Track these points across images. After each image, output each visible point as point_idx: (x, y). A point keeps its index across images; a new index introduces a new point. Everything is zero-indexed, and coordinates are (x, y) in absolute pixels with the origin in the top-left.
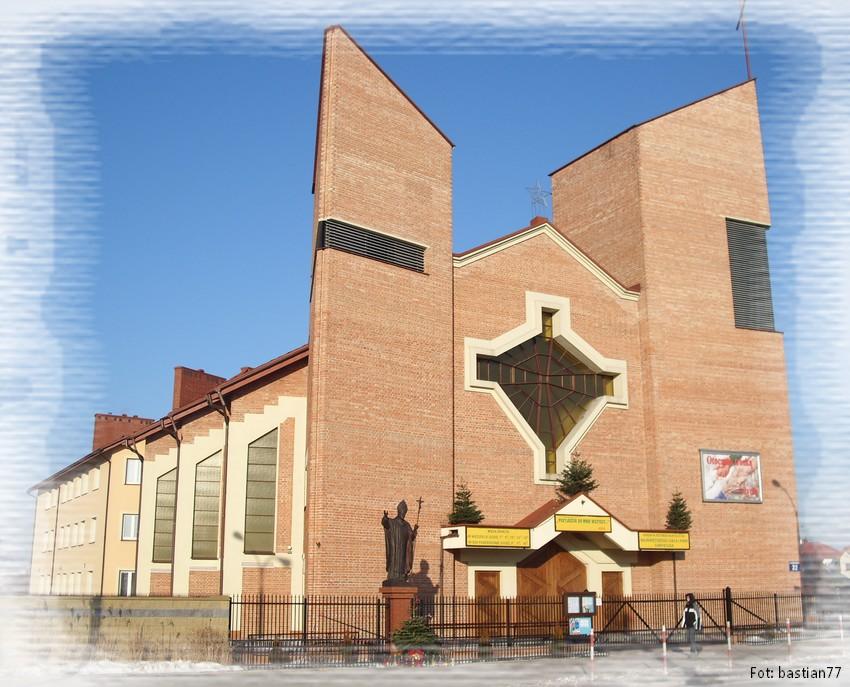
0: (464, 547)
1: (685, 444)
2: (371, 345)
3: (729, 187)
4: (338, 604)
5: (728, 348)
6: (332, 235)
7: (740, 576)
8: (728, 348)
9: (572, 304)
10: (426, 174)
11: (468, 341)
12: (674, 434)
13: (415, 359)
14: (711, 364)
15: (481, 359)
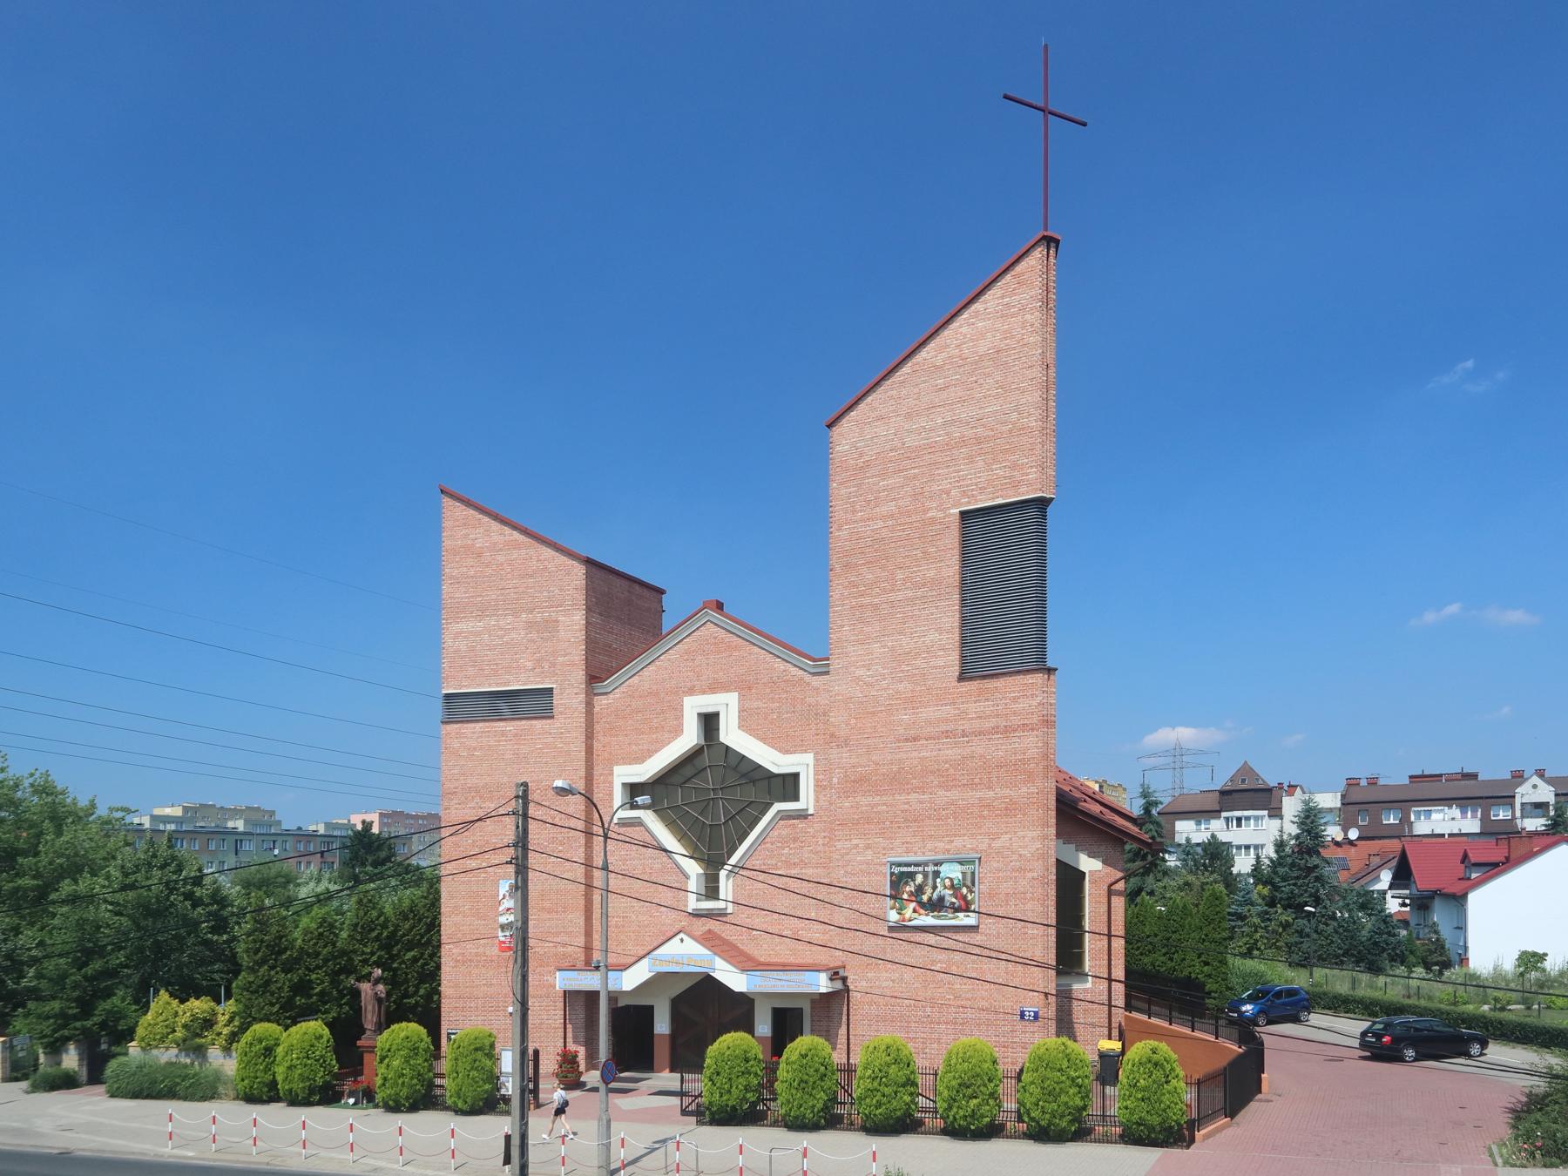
1: (869, 851)
3: (971, 459)
4: (926, 1074)
6: (460, 707)
7: (939, 1023)
9: (741, 699)
10: (552, 606)
11: (618, 770)
12: (855, 842)
14: (915, 739)
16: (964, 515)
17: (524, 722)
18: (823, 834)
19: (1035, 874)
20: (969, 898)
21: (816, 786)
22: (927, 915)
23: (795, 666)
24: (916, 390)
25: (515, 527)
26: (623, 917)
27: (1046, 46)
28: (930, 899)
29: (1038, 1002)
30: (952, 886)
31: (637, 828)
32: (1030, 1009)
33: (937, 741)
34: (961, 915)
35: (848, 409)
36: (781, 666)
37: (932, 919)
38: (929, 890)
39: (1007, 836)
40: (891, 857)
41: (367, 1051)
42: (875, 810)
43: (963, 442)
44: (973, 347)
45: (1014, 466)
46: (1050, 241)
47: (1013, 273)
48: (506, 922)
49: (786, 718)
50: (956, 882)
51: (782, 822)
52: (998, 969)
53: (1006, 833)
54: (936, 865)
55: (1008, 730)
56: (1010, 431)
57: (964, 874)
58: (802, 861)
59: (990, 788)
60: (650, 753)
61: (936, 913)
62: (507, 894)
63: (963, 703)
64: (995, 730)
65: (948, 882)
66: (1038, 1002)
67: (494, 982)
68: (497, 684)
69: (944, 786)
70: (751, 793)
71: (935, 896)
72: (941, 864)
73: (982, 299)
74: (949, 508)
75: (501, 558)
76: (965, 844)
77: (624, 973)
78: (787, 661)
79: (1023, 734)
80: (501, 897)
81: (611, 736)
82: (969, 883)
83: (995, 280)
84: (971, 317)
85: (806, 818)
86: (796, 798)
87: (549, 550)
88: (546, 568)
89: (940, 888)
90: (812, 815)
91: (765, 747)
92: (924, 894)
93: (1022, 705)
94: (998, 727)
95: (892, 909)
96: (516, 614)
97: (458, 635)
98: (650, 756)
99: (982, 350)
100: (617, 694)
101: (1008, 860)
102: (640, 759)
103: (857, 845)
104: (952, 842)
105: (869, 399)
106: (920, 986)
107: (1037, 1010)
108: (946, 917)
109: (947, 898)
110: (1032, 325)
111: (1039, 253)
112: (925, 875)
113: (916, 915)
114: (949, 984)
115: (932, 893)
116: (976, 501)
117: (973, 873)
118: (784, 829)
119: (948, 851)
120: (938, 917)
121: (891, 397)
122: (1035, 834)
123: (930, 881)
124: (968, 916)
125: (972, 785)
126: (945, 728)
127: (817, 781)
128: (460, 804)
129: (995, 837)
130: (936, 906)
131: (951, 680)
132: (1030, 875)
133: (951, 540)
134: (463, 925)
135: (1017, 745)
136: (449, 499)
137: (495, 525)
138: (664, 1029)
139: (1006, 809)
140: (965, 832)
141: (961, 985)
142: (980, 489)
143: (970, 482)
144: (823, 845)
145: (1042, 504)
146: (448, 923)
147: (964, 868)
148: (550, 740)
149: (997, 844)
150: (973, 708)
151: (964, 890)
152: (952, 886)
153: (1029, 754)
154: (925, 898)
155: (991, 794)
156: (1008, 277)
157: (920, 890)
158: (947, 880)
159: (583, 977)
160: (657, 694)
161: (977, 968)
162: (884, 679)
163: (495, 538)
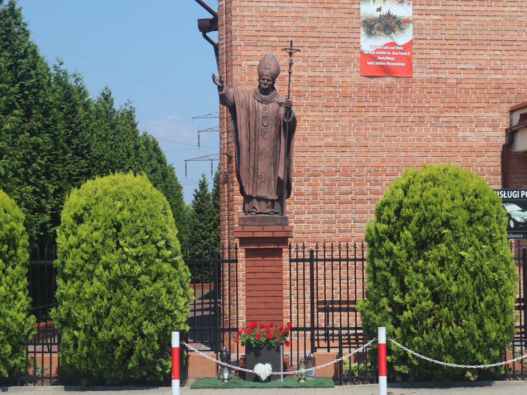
48: (377, 15)
67: (352, 140)
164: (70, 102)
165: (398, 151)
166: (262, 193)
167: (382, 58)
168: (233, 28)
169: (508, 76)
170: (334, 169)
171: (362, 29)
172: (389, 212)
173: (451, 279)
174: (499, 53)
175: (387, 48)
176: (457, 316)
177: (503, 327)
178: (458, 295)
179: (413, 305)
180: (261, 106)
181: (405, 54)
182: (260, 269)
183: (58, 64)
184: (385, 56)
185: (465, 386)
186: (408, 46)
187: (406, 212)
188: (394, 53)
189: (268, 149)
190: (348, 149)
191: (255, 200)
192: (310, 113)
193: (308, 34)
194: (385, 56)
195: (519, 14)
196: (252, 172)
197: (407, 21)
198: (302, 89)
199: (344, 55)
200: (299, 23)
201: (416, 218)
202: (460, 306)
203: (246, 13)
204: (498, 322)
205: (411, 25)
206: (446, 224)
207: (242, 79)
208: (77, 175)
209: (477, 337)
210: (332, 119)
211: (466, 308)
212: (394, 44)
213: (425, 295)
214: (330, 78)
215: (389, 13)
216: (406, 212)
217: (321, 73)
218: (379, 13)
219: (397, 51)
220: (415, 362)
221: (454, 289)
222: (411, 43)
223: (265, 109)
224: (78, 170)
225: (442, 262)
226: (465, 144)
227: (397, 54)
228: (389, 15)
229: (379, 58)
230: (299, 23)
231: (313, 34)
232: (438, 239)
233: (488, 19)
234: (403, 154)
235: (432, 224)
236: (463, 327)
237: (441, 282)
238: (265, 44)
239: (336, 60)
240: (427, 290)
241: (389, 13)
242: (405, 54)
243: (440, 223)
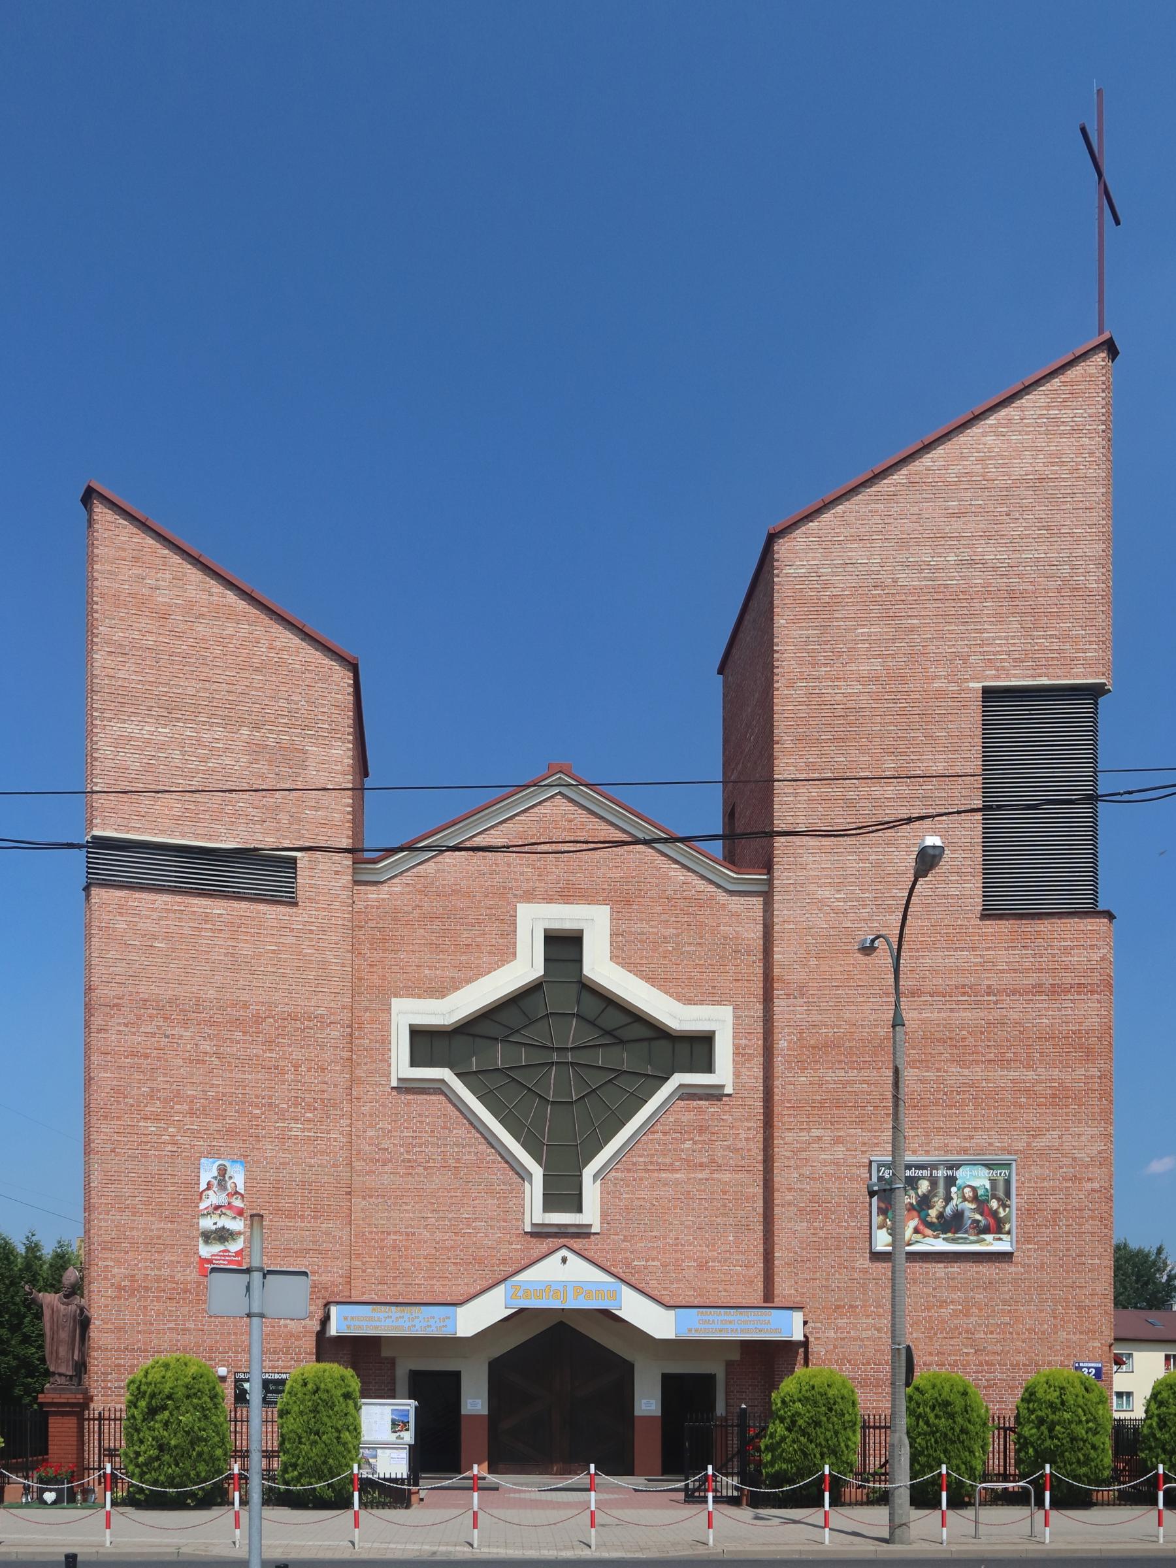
0: (674, 1338)
1: (841, 1148)
2: (177, 1031)
3: (999, 618)
5: (963, 957)
8: (963, 957)
9: (615, 917)
10: (295, 726)
11: (397, 1004)
12: (816, 1133)
13: (269, 1042)
15: (417, 1033)
16: (989, 694)
17: (244, 905)
18: (746, 1124)
19: (1096, 1185)
20: (1002, 1214)
21: (736, 1054)
22: (936, 1237)
23: (703, 877)
24: (915, 510)
25: (229, 584)
26: (407, 1234)
27: (1099, 91)
28: (941, 1215)
29: (1100, 1355)
30: (975, 1198)
31: (432, 1097)
32: (1090, 1365)
33: (948, 998)
34: (989, 1237)
35: (806, 517)
36: (681, 875)
37: (945, 1242)
38: (939, 1203)
39: (1056, 1133)
40: (876, 1155)
41: (56, 1413)
42: (848, 1089)
43: (987, 592)
44: (1004, 465)
45: (1064, 637)
46: (1111, 348)
47: (1062, 378)
48: (214, 1227)
49: (688, 952)
50: (981, 1192)
51: (682, 1103)
52: (1041, 1311)
53: (1054, 1129)
54: (950, 1168)
55: (1056, 991)
56: (1059, 590)
57: (993, 1182)
58: (713, 1161)
59: (1028, 1067)
60: (457, 985)
61: (949, 1235)
62: (215, 1182)
63: (988, 949)
64: (1037, 989)
65: (968, 1192)
66: (1100, 1355)
67: (191, 1325)
68: (197, 836)
69: (961, 1062)
70: (625, 1059)
71: (949, 1211)
72: (958, 1166)
73: (1018, 403)
74: (967, 680)
75: (203, 630)
76: (990, 1141)
77: (461, 1311)
78: (689, 869)
79: (1079, 997)
80: (203, 1186)
81: (384, 951)
82: (1001, 1194)
83: (1038, 383)
84: (1000, 425)
85: (720, 1100)
86: (709, 1068)
87: (291, 636)
88: (282, 663)
89: (956, 1200)
90: (729, 1095)
91: (655, 991)
92: (931, 1207)
93: (1078, 958)
94: (1041, 985)
95: (880, 1227)
96: (230, 725)
97: (121, 742)
98: (458, 989)
99: (1017, 473)
100: (397, 886)
101: (1056, 1165)
102: (440, 991)
103: (820, 1138)
104: (971, 1137)
105: (839, 509)
106: (921, 1336)
107: (1100, 1365)
108: (965, 1241)
109: (967, 1214)
110: (1091, 454)
111: (1100, 358)
112: (934, 1182)
113: (918, 1237)
114: (967, 1332)
115: (944, 1207)
116: (1008, 676)
117: (1008, 1182)
118: (686, 1113)
119: (965, 1151)
120: (954, 1241)
121: (874, 513)
122: (1095, 1131)
123: (941, 1190)
124: (1000, 1239)
125: (1001, 1061)
126: (961, 981)
127: (736, 1047)
128: (126, 1025)
129: (1037, 1133)
130: (951, 1224)
131: (970, 916)
132: (1089, 1186)
133: (971, 721)
134: (132, 1229)
135: (1070, 1012)
136: (106, 510)
137: (194, 574)
138: (479, 1407)
139: (1054, 1096)
140: (992, 1125)
141: (985, 1333)
142: (1015, 660)
143: (998, 649)
144: (747, 1139)
145: (1095, 692)
146: (103, 1224)
147: (994, 1173)
148: (290, 940)
149: (1041, 1143)
150: (1003, 957)
151: (994, 1204)
152: (975, 1198)
153: (1087, 1024)
154: (933, 1213)
155: (1031, 1075)
156: (1056, 382)
157: (925, 1202)
158: (967, 1190)
159: (381, 1315)
160: (468, 894)
161: (1010, 1311)
162: (864, 906)
163: (193, 593)
164: (31, 1272)
165: (229, 1334)
166: (62, 1370)
167: (217, 1262)
168: (91, 1235)
169: (323, 1278)
170: (175, 1348)
171: (200, 1239)
172: (133, 1387)
173: (172, 1436)
174: (316, 1259)
175: (221, 1254)
176: (175, 1460)
177: (212, 1469)
178: (176, 1447)
179: (145, 1453)
180: (62, 1307)
181: (237, 1259)
182: (60, 1425)
183: (30, 1235)
184: (219, 1260)
185: (189, 1510)
186: (238, 1253)
187: (143, 1388)
188: (227, 1258)
189: (67, 1339)
190: (1070, 1196)
191: (57, 1376)
192: (155, 1304)
193: (155, 1241)
194: (219, 1260)
195: (333, 1229)
196: (54, 1354)
197: (239, 1233)
198: (149, 1284)
199: (185, 1258)
200: (148, 1232)
201: (148, 1393)
202: (178, 1454)
203: (103, 1224)
204: (208, 1466)
205: (242, 1236)
206: (169, 1397)
207: (99, 1276)
208: (36, 1337)
209: (192, 1476)
210: (174, 1309)
211: (182, 1456)
212: (228, 1251)
213: (153, 1446)
214: (173, 1277)
215: (224, 1227)
216: (143, 1388)
217: (166, 1272)
218: (215, 1226)
219: (231, 1256)
220: (147, 1492)
221: (173, 1442)
222: (242, 1250)
223: (65, 1309)
224: (36, 1332)
225: (166, 1424)
226: (286, 1330)
227: (229, 1258)
228: (223, 1228)
229: (214, 1262)
230: (148, 1232)
231: (159, 1242)
232: (164, 1408)
233: (307, 1233)
234: (233, 1337)
235: (159, 1397)
236: (180, 1468)
237: (163, 1437)
238: (118, 1248)
239: (178, 1262)
240: (154, 1443)
241: (224, 1227)
242: (237, 1259)
243: (165, 1396)
